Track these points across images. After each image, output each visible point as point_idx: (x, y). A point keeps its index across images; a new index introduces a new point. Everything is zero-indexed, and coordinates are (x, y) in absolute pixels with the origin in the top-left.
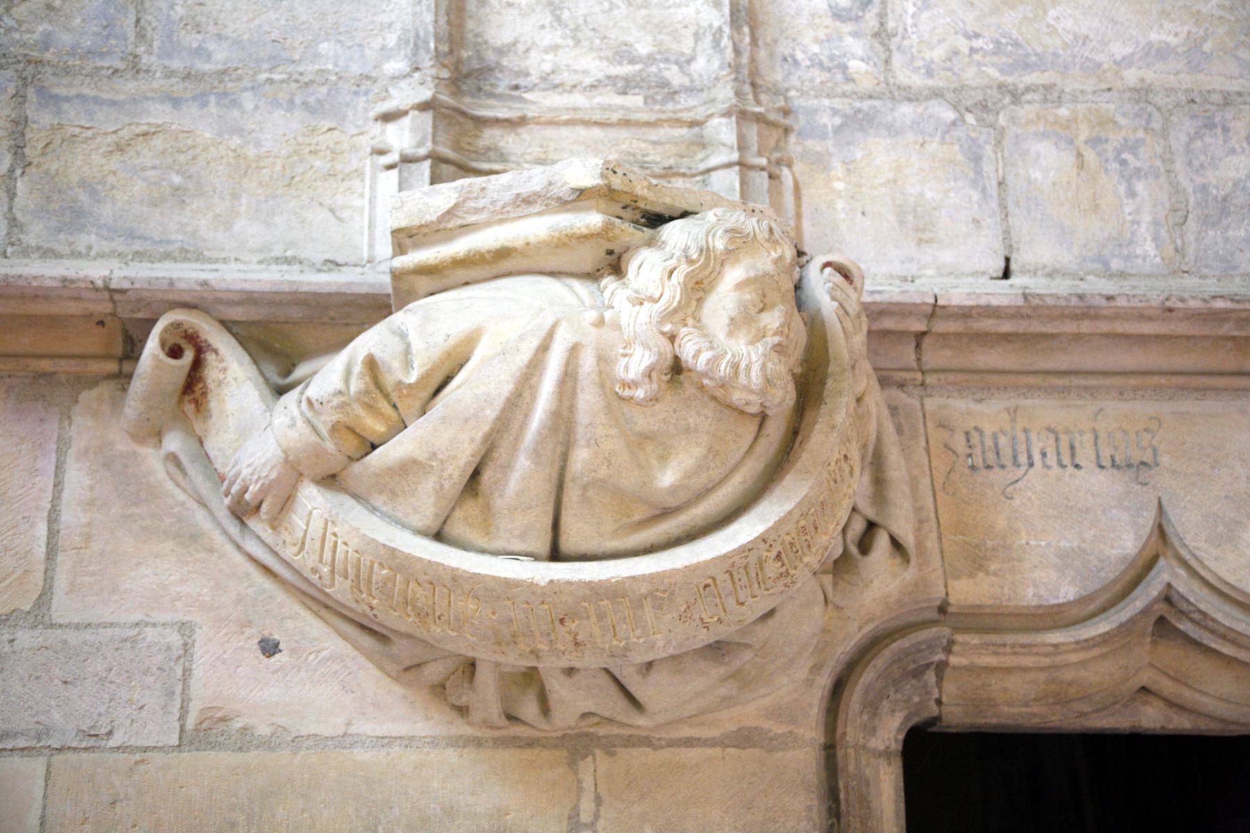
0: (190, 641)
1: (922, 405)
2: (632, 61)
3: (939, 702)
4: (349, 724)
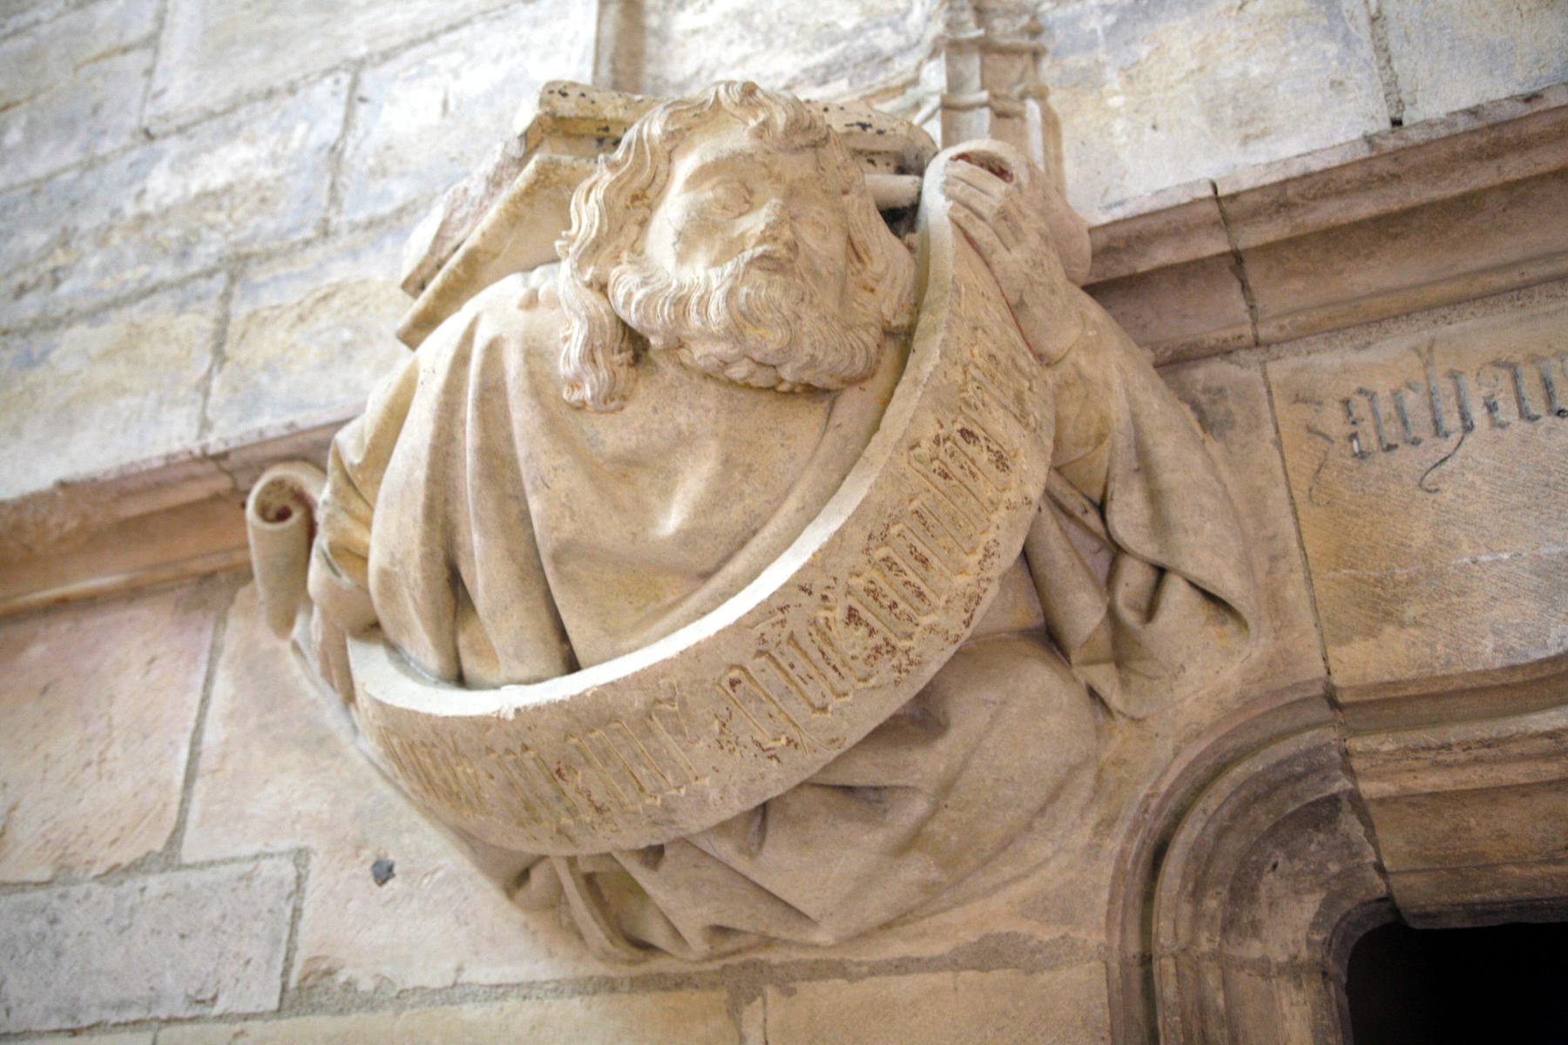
0: (303, 872)
1: (1265, 375)
2: (834, 42)
3: (1380, 869)
4: (459, 970)
